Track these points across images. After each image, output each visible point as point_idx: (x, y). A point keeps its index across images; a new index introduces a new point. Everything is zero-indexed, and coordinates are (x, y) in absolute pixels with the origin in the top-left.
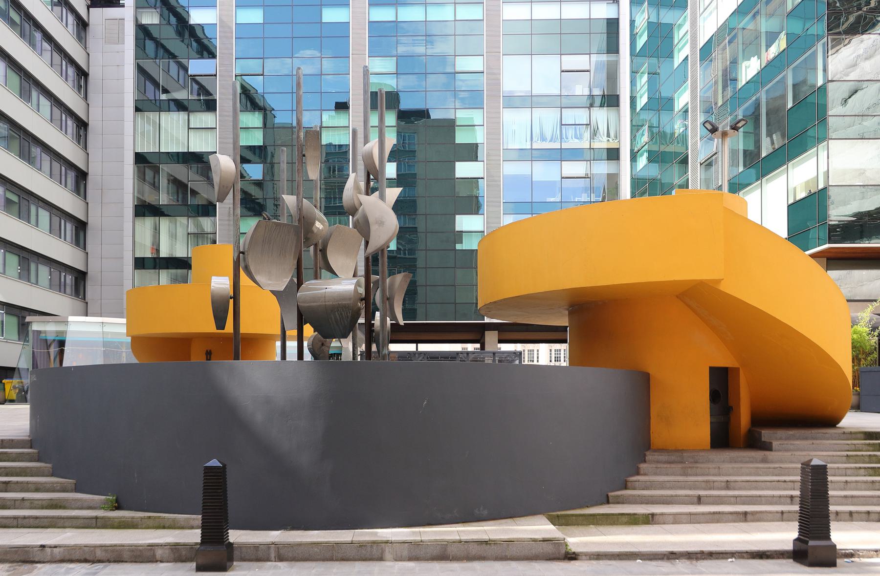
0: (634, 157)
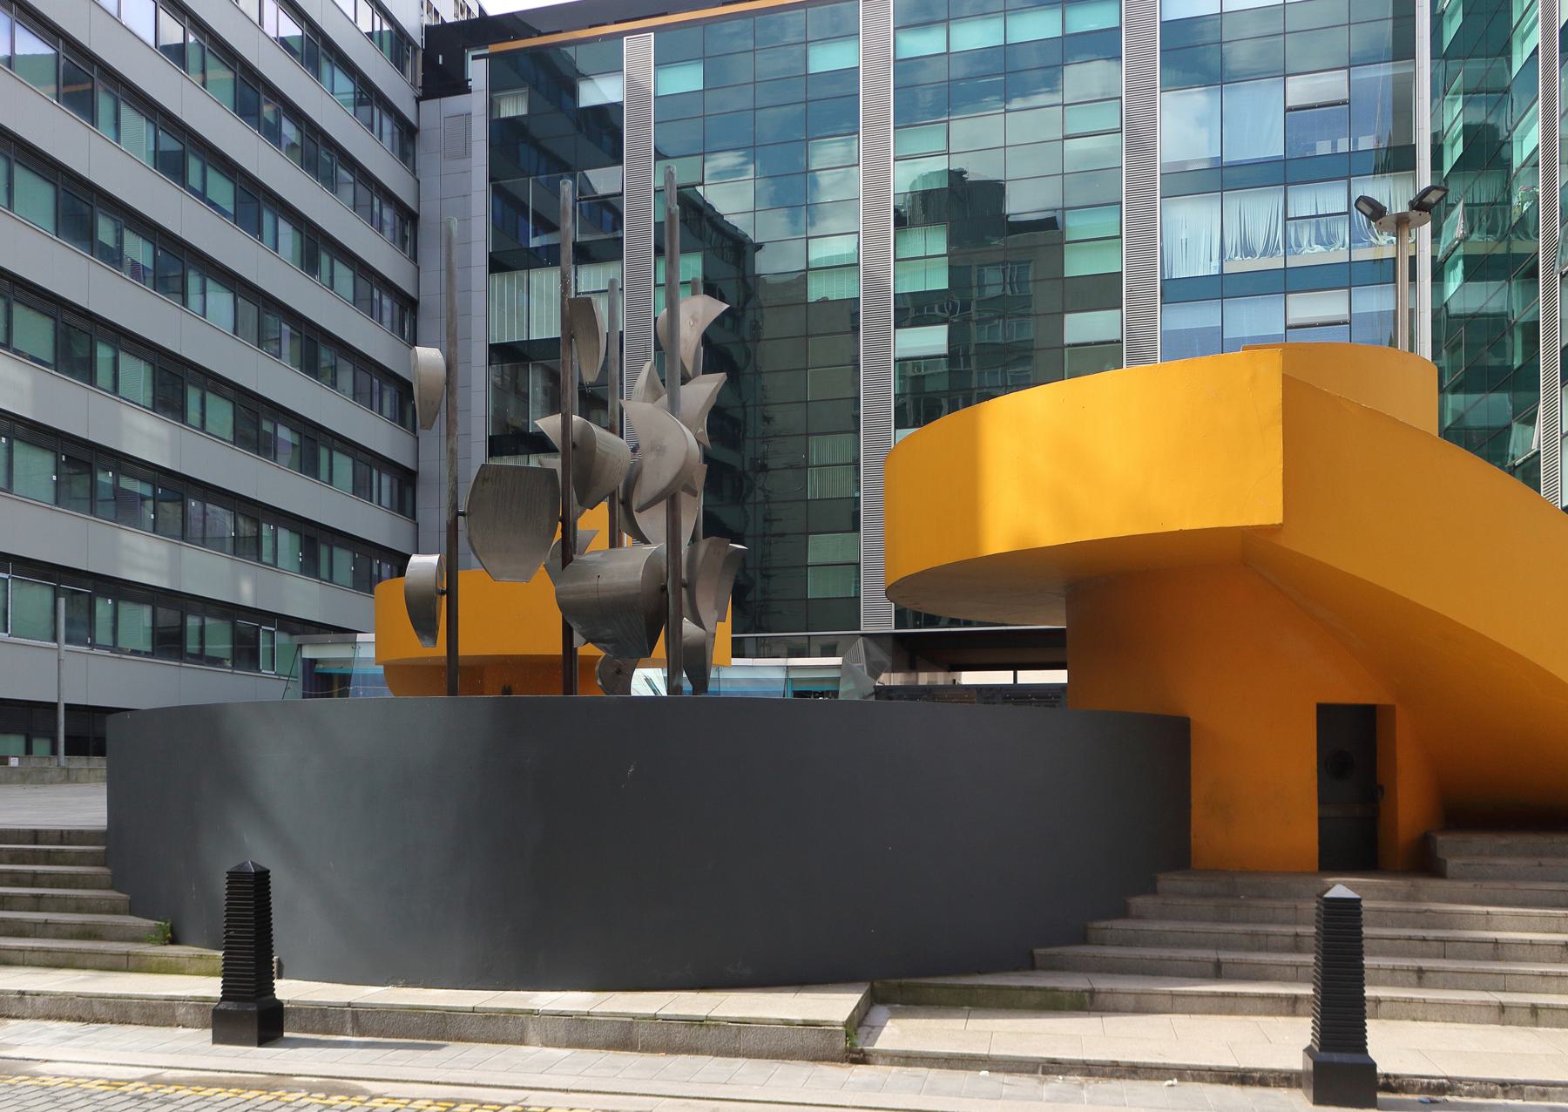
0: (1438, 275)
